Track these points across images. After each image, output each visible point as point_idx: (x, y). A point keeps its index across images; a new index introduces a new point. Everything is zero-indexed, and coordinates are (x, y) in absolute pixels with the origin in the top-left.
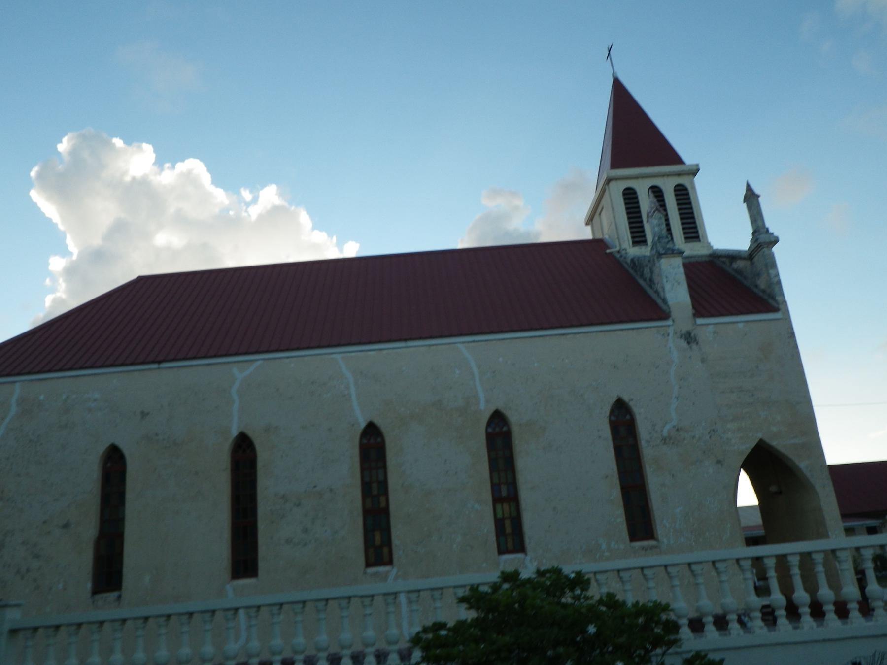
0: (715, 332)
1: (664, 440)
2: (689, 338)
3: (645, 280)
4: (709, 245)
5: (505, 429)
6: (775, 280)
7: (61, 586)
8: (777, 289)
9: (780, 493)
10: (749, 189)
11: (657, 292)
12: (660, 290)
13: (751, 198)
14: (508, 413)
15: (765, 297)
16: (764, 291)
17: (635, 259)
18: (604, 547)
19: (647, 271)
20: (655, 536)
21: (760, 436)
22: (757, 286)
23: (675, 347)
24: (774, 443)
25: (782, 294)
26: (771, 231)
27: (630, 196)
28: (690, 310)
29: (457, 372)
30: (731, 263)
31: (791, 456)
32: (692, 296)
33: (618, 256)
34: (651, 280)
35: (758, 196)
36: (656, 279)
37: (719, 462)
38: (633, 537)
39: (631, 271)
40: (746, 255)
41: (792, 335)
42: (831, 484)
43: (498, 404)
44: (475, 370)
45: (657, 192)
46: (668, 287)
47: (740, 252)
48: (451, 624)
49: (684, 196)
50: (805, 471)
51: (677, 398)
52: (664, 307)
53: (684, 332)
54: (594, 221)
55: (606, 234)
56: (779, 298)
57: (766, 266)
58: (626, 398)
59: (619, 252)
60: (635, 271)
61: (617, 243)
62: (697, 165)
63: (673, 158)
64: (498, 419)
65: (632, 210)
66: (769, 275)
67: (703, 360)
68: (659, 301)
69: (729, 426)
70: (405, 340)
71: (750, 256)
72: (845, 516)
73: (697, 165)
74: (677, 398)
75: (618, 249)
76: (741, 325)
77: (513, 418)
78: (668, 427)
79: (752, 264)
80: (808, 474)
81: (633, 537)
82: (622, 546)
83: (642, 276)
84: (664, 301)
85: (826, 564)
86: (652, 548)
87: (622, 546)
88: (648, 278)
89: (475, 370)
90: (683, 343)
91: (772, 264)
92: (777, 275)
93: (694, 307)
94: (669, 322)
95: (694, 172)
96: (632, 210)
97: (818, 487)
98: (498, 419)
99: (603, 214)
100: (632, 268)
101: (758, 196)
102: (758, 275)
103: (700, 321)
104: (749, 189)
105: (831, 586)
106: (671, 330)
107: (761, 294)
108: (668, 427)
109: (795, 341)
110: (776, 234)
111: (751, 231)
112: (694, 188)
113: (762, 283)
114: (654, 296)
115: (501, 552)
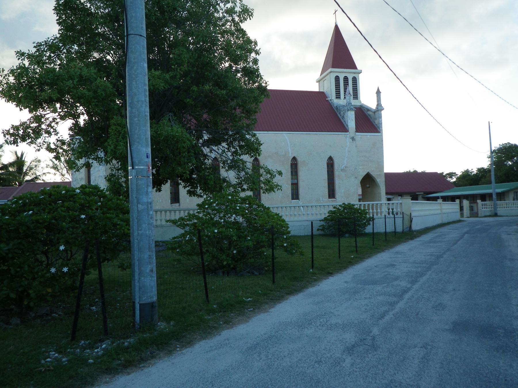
0: (361, 138)
1: (342, 170)
2: (353, 139)
3: (341, 115)
4: (360, 102)
5: (295, 162)
6: (380, 122)
7: (161, 201)
8: (381, 125)
9: (369, 187)
10: (378, 90)
11: (345, 121)
12: (346, 121)
13: (378, 92)
14: (297, 157)
15: (377, 127)
16: (376, 125)
17: (338, 107)
18: (321, 200)
19: (342, 113)
20: (335, 197)
21: (368, 171)
22: (374, 122)
23: (348, 140)
24: (371, 173)
25: (382, 127)
26: (382, 106)
27: (337, 79)
28: (354, 130)
29: (283, 143)
30: (367, 111)
31: (375, 177)
32: (356, 125)
33: (331, 102)
34: (343, 116)
35: (381, 93)
36: (345, 117)
37: (356, 178)
38: (329, 197)
39: (336, 110)
40: (374, 111)
41: (383, 145)
42: (385, 186)
43: (295, 155)
44: (289, 143)
45: (346, 79)
46: (349, 121)
47: (371, 108)
48: (459, 173)
49: (355, 80)
50: (378, 182)
51: (347, 157)
52: (347, 128)
53: (352, 137)
54: (320, 82)
55: (325, 90)
56: (380, 128)
57: (379, 117)
58: (332, 156)
59: (331, 100)
60: (337, 111)
61: (330, 97)
62: (361, 70)
63: (354, 67)
64: (294, 159)
65: (337, 85)
66: (379, 120)
67: (356, 146)
68: (345, 125)
69: (360, 167)
70: (268, 131)
71: (374, 112)
72: (387, 194)
73: (361, 70)
74: (347, 157)
75: (330, 99)
76: (368, 136)
77: (299, 160)
78: (343, 166)
79: (375, 114)
80: (379, 183)
81: (329, 197)
82: (326, 200)
83: (340, 113)
84: (347, 125)
85: (380, 206)
86: (334, 201)
87: (326, 200)
88: (342, 116)
89: (289, 143)
90: (351, 140)
91: (380, 117)
92: (382, 121)
93: (356, 129)
94: (348, 133)
95: (360, 72)
96: (337, 85)
97: (381, 187)
98: (294, 159)
99: (325, 82)
100: (336, 109)
101: (381, 93)
102: (376, 119)
103: (357, 134)
104: (378, 90)
105: (380, 210)
106: (348, 136)
107: (375, 125)
108: (343, 166)
109: (383, 143)
110: (383, 107)
111: (377, 104)
112: (359, 79)
113: (376, 122)
114: (344, 123)
115: (292, 199)
